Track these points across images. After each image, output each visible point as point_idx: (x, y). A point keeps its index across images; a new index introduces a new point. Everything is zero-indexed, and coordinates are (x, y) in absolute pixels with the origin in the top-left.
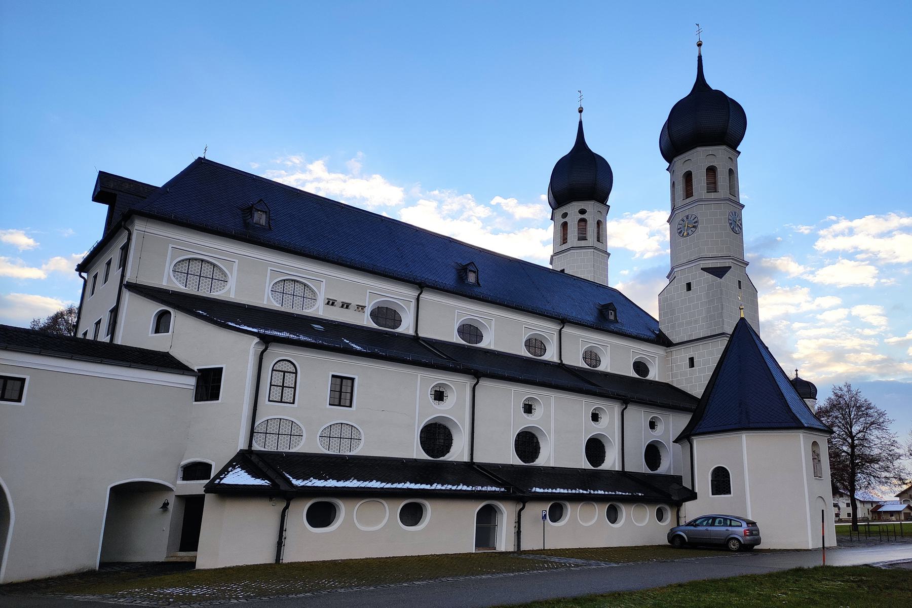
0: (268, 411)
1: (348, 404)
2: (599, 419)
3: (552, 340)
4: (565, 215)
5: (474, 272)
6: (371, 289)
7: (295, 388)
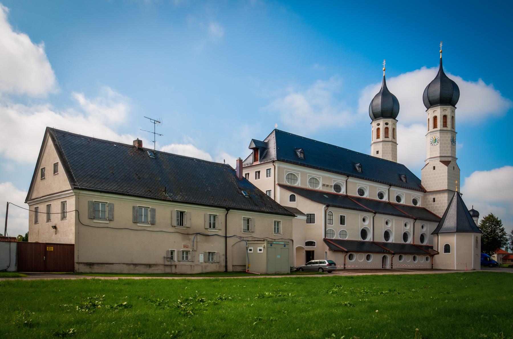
1: (89, 202)
3: (386, 193)
4: (379, 125)
6: (334, 179)
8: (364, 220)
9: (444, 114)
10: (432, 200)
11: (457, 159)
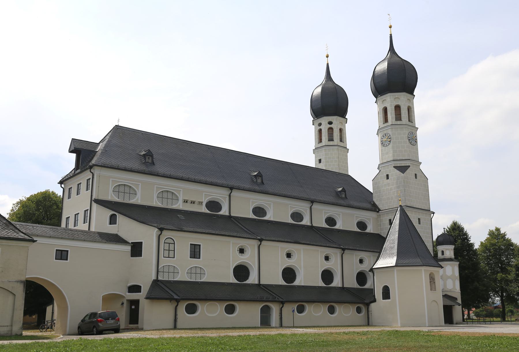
0: (164, 262)
1: (198, 257)
2: (329, 259)
4: (320, 124)
5: (260, 176)
7: (174, 251)
8: (242, 251)
10: (388, 221)
11: (421, 163)
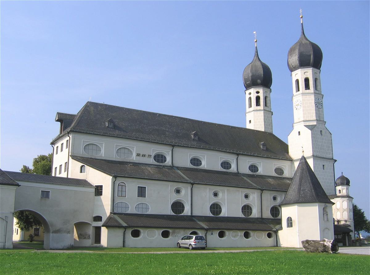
1: (144, 196)
9: (305, 76)
